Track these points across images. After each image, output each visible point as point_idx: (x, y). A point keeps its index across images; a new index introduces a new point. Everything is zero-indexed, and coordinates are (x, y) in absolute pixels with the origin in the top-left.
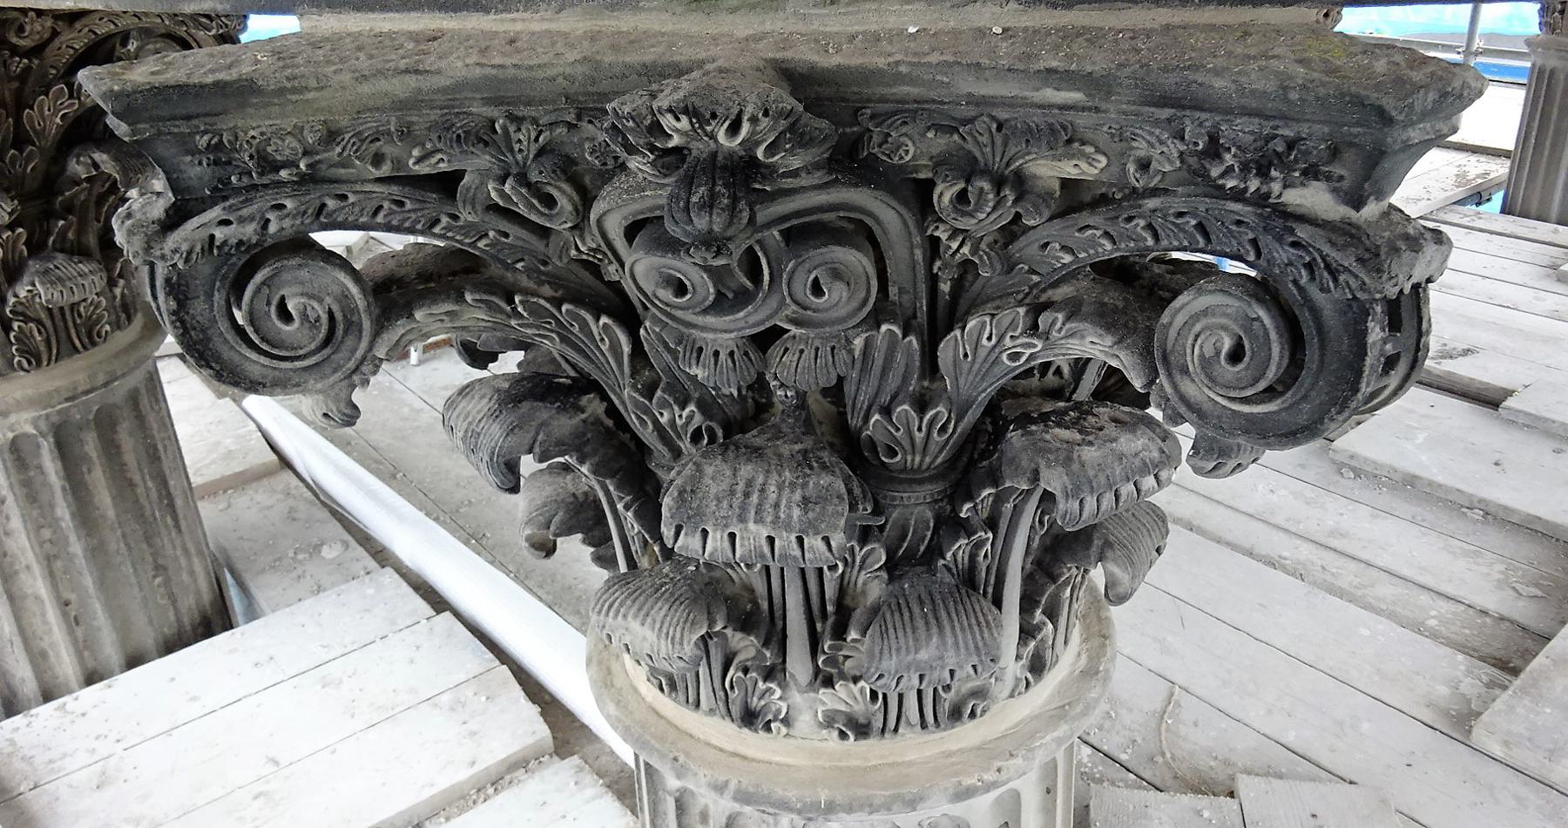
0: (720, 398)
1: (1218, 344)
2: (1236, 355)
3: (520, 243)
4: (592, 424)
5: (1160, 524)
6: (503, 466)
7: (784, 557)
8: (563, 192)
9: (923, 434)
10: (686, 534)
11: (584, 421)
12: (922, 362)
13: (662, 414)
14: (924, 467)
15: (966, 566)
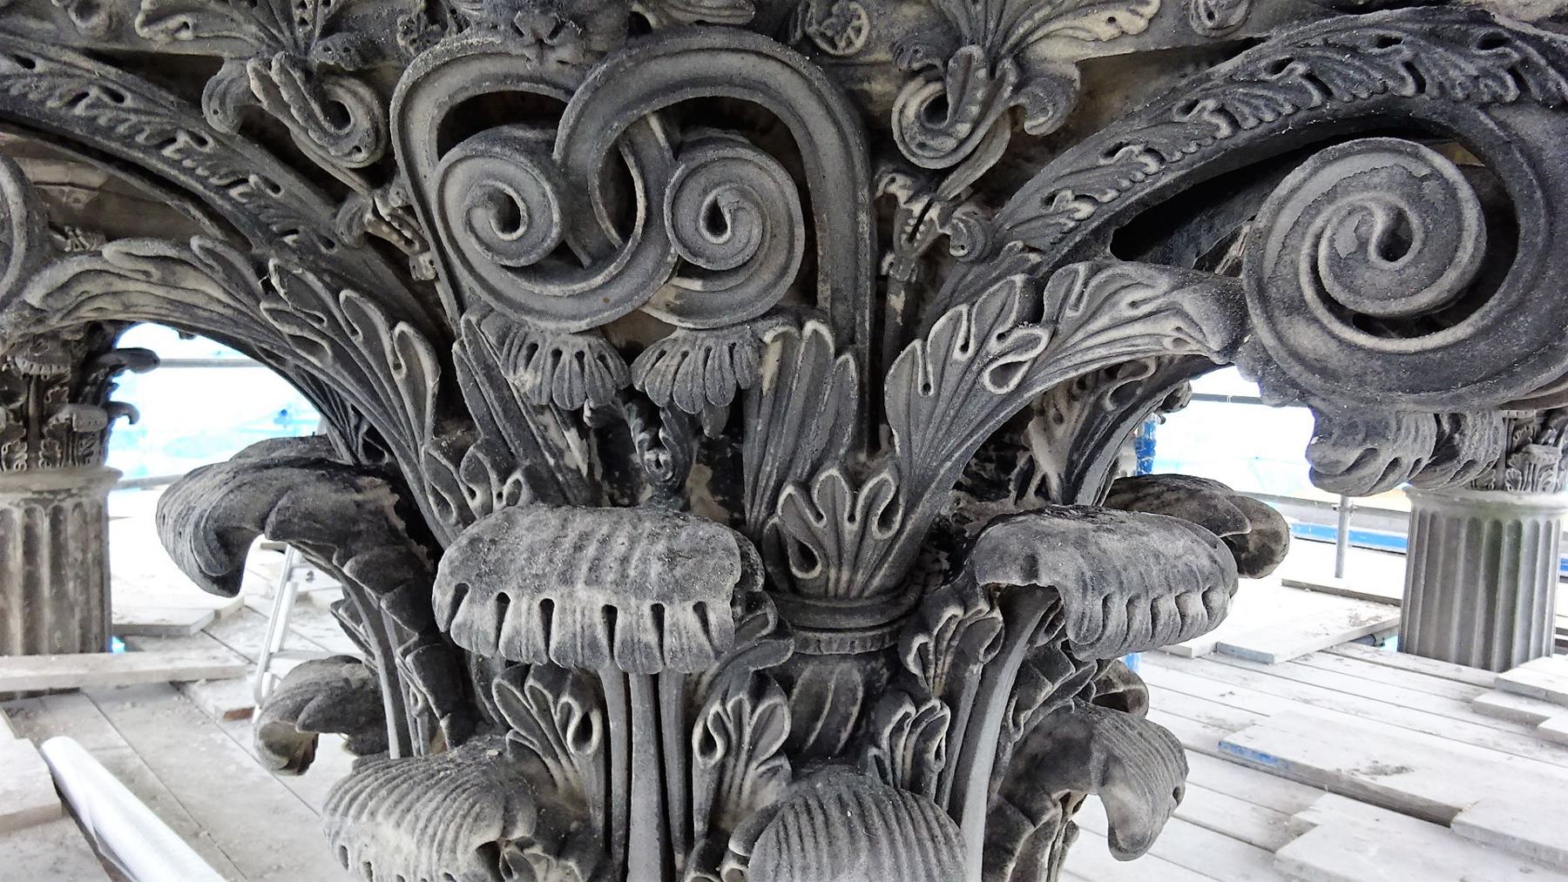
0: (561, 471)
1: (1363, 229)
2: (1394, 246)
3: (296, 204)
4: (370, 512)
5: (1178, 755)
6: (212, 536)
7: (632, 646)
8: (361, 100)
9: (855, 527)
10: (472, 601)
11: (359, 505)
12: (861, 404)
13: (473, 494)
14: (854, 593)
15: (907, 777)
